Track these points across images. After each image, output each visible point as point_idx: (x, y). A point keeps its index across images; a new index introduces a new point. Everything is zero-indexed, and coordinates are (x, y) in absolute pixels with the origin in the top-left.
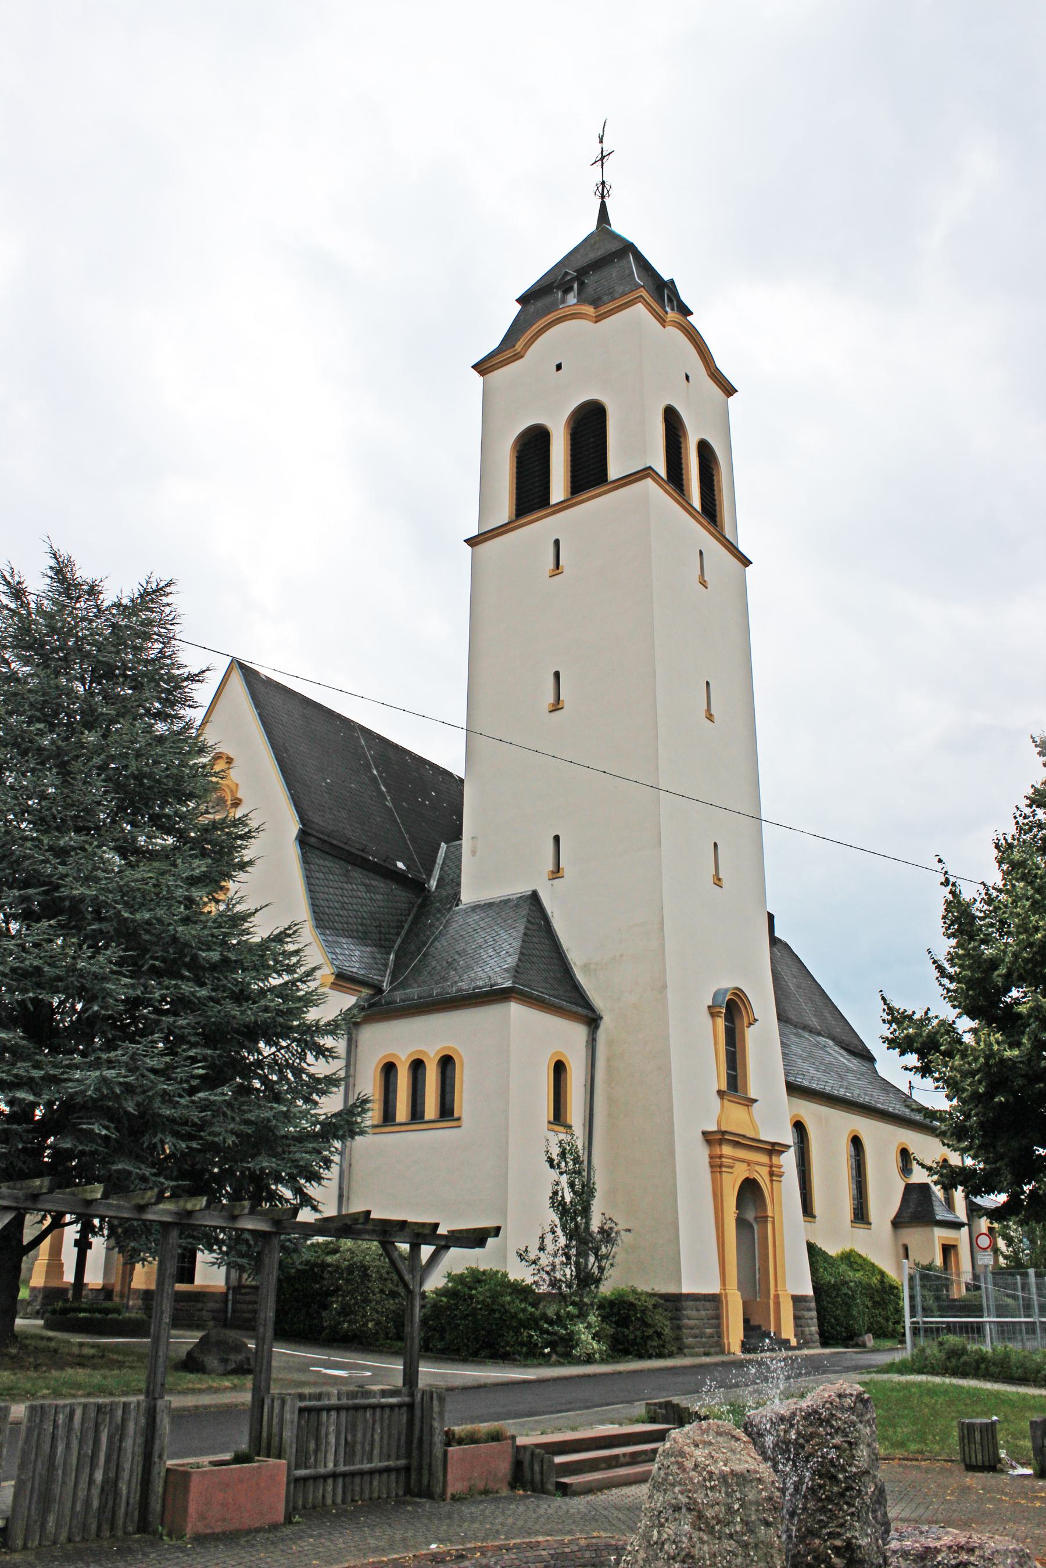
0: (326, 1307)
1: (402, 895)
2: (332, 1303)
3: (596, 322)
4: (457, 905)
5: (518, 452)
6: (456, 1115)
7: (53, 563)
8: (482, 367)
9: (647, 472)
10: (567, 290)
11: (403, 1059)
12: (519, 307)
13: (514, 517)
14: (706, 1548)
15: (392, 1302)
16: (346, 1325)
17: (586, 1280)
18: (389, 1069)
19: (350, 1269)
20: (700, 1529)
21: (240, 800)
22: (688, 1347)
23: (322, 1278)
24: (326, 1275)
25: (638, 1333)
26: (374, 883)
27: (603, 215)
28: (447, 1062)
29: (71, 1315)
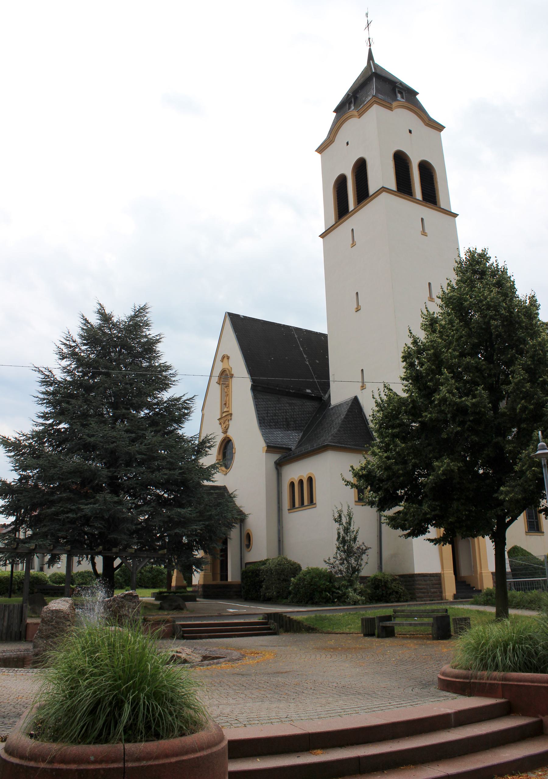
0: (261, 587)
1: (316, 404)
2: (263, 585)
3: (359, 118)
4: (330, 406)
5: (337, 188)
6: (314, 502)
7: (99, 307)
8: (321, 150)
9: (384, 189)
11: (296, 479)
12: (335, 114)
13: (338, 220)
14: (44, 627)
15: (285, 583)
16: (268, 594)
17: (355, 570)
18: (292, 484)
19: (267, 571)
20: (43, 623)
21: (233, 375)
22: (419, 597)
23: (259, 575)
24: (260, 574)
25: (384, 592)
26: (293, 402)
27: (370, 57)
28: (310, 480)
29: (163, 594)
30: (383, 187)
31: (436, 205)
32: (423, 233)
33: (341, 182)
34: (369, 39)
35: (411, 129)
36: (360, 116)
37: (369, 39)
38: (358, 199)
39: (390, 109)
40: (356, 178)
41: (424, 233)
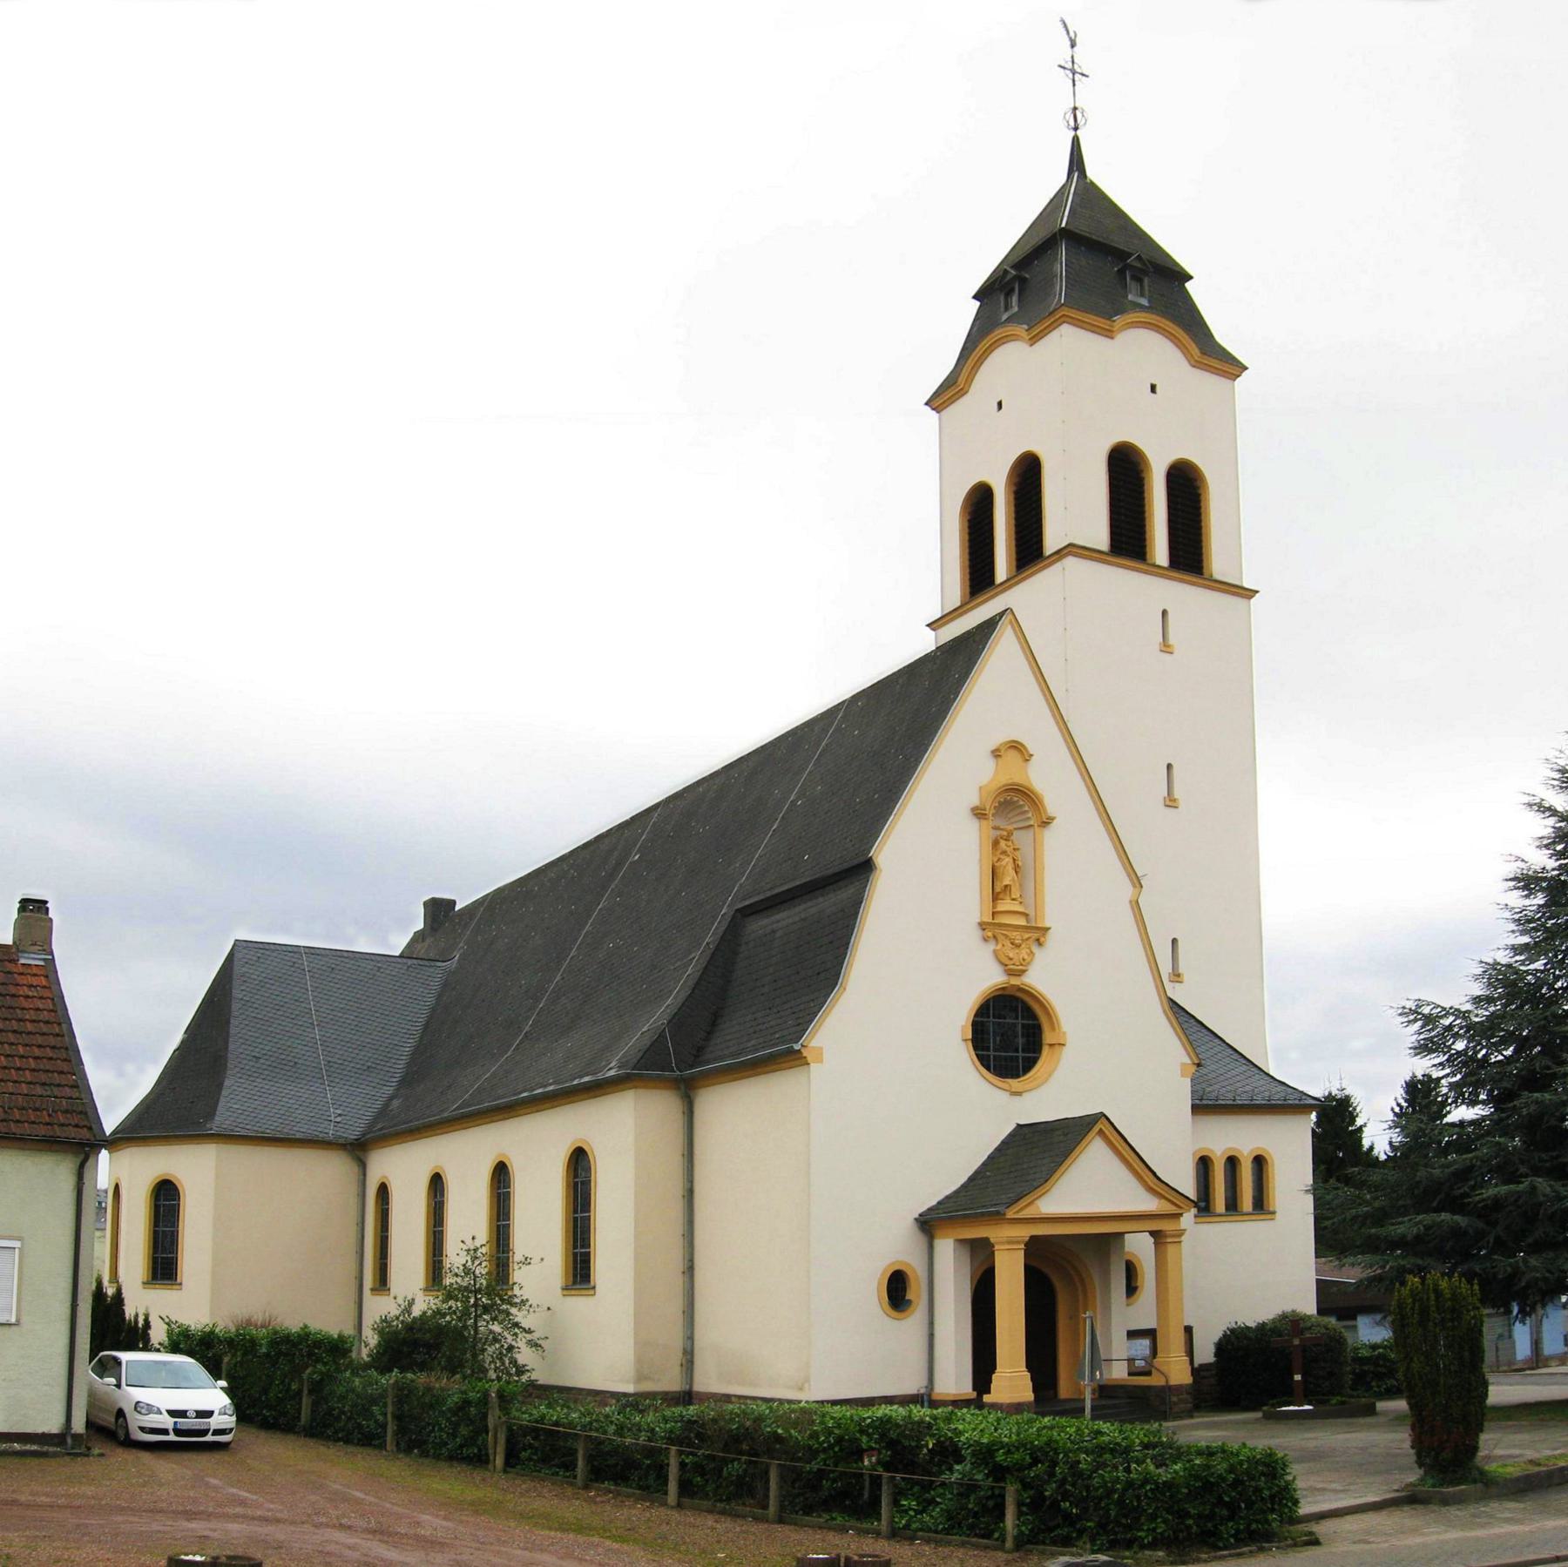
3: (1031, 345)
8: (944, 396)
9: (1071, 550)
10: (1009, 294)
12: (978, 304)
27: (1076, 162)
30: (1070, 545)
31: (1202, 574)
32: (1164, 649)
33: (979, 503)
34: (1075, 109)
35: (1153, 395)
36: (1033, 340)
37: (1075, 109)
38: (1018, 560)
39: (1109, 334)
40: (1016, 499)
41: (1166, 647)
